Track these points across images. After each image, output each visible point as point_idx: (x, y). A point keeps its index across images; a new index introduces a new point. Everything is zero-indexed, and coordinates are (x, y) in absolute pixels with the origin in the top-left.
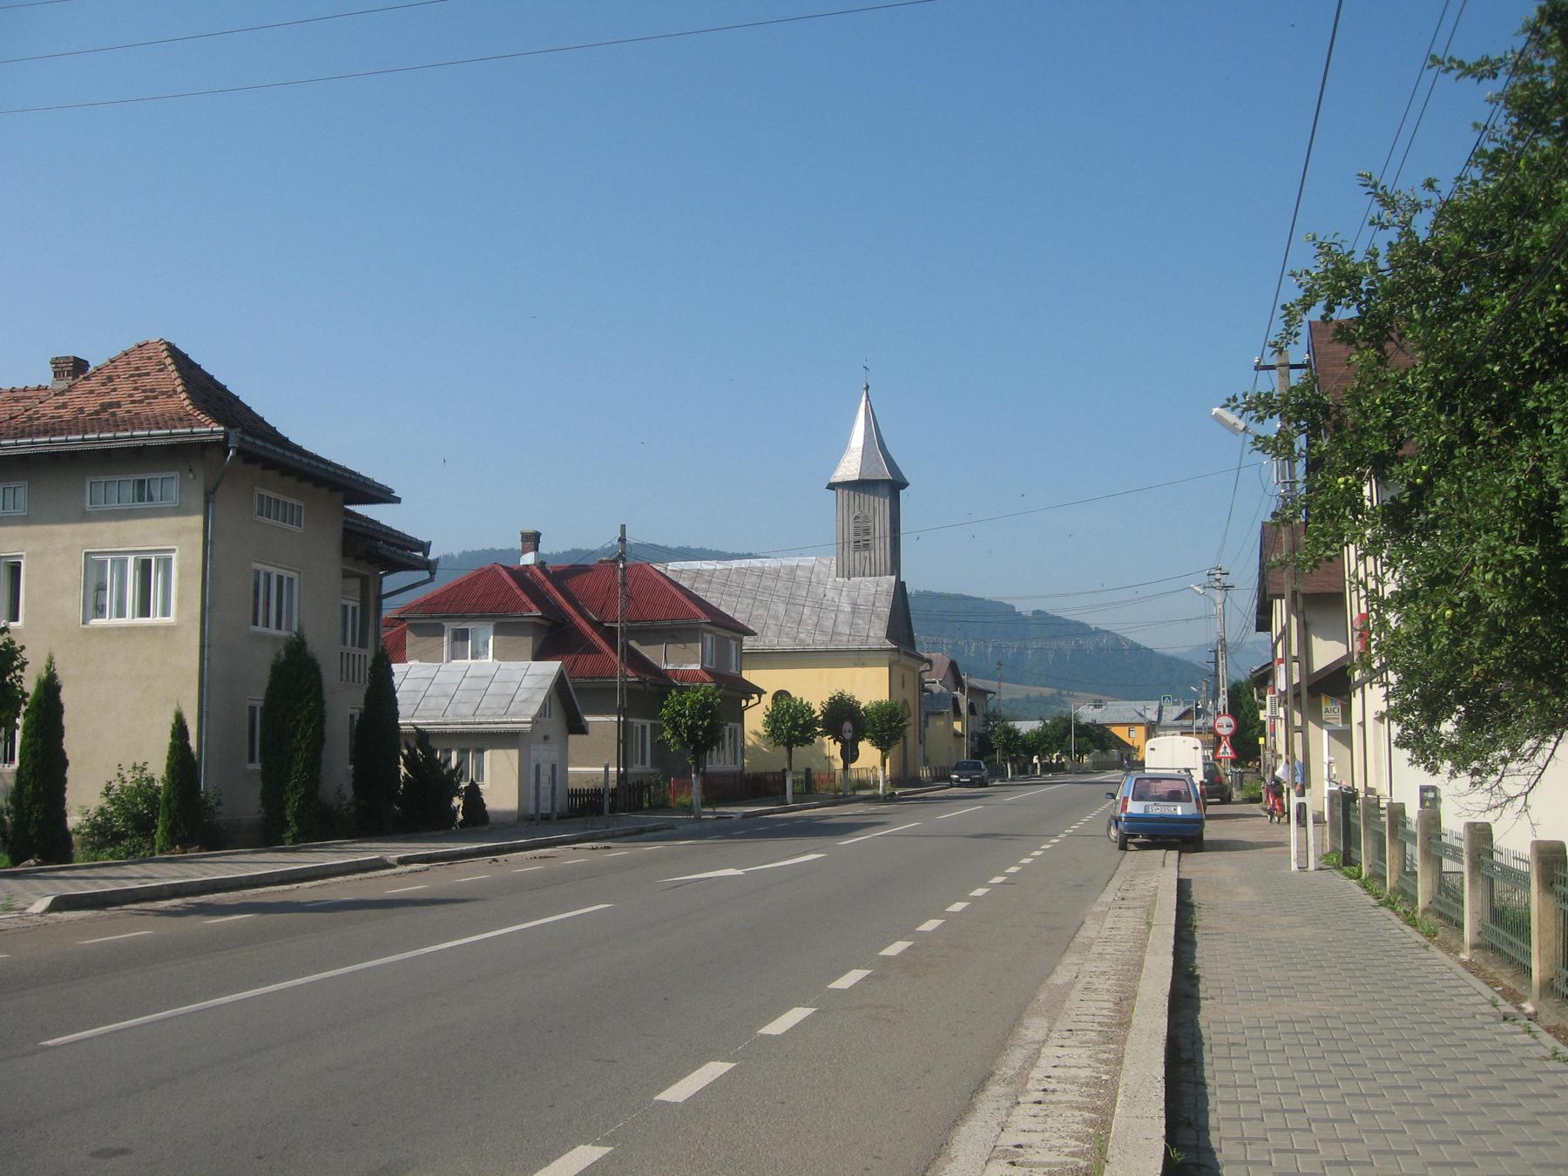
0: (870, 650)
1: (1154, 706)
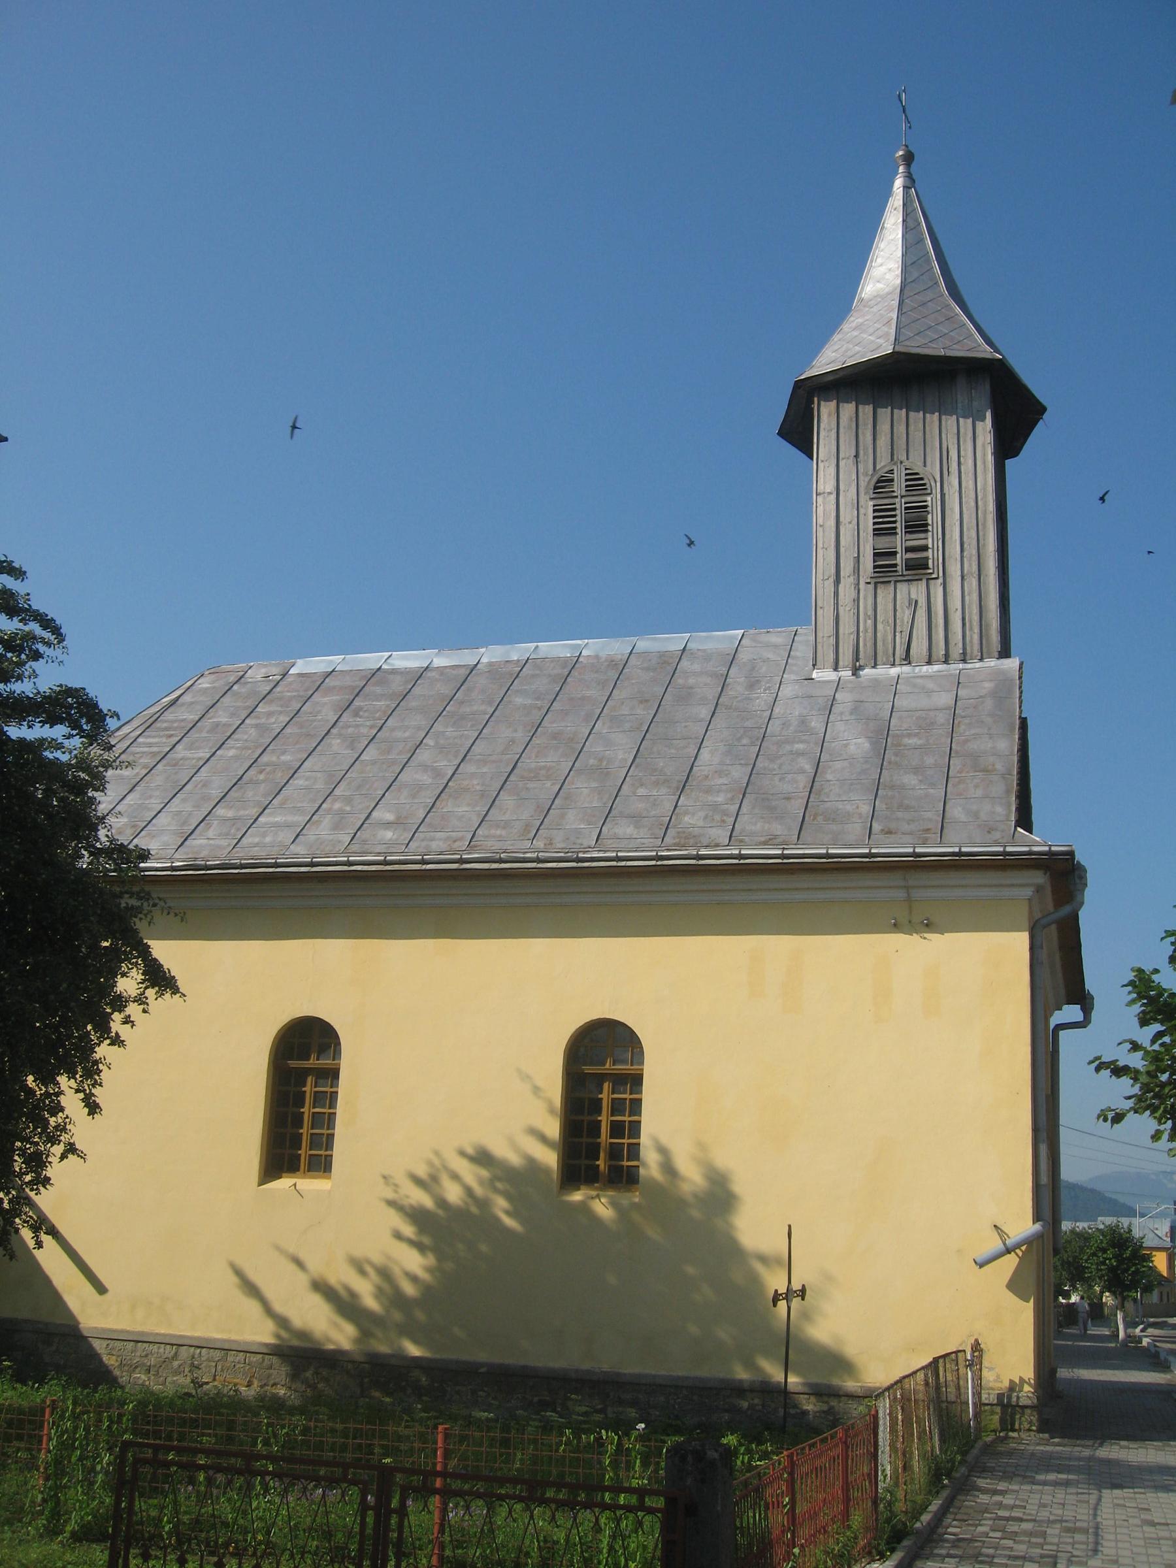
0: (961, 863)
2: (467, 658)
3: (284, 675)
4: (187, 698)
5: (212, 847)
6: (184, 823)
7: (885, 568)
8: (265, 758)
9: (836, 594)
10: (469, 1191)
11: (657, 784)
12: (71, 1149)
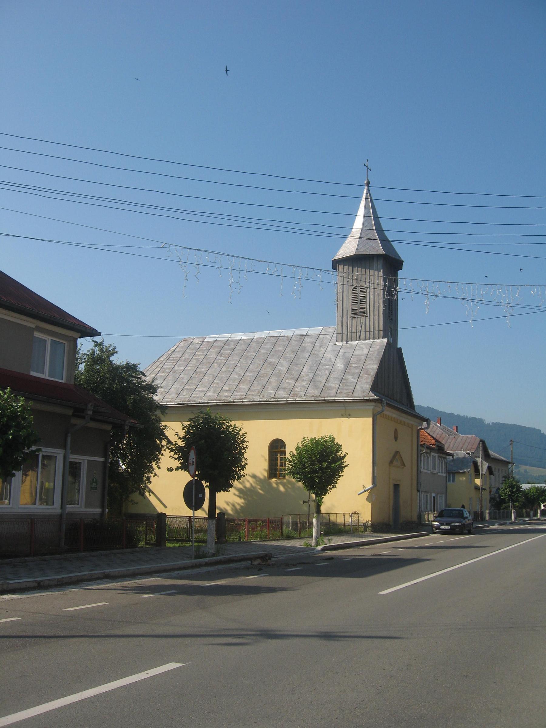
0: (354, 401)
2: (250, 336)
3: (203, 342)
6: (177, 391)
8: (198, 370)
9: (342, 321)
10: (251, 484)
11: (291, 379)
12: (155, 475)
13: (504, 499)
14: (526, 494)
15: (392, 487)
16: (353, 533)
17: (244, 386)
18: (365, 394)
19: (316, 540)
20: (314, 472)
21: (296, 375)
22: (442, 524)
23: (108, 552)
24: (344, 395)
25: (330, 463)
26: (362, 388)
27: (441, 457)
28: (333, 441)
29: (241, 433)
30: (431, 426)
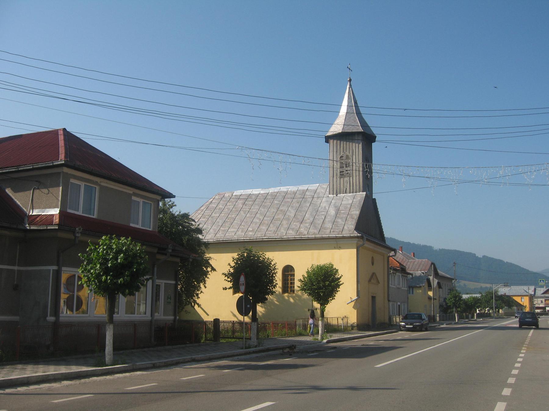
0: (343, 238)
1: (532, 288)
4: (214, 201)
5: (220, 236)
7: (342, 175)
11: (297, 222)
12: (202, 292)
13: (450, 306)
14: (465, 302)
15: (370, 298)
16: (344, 331)
17: (264, 228)
18: (351, 232)
19: (321, 336)
20: (320, 288)
21: (300, 218)
22: (407, 324)
23: (184, 346)
24: (336, 233)
25: (331, 282)
26: (348, 228)
27: (404, 276)
28: (332, 267)
29: (273, 263)
30: (398, 254)
